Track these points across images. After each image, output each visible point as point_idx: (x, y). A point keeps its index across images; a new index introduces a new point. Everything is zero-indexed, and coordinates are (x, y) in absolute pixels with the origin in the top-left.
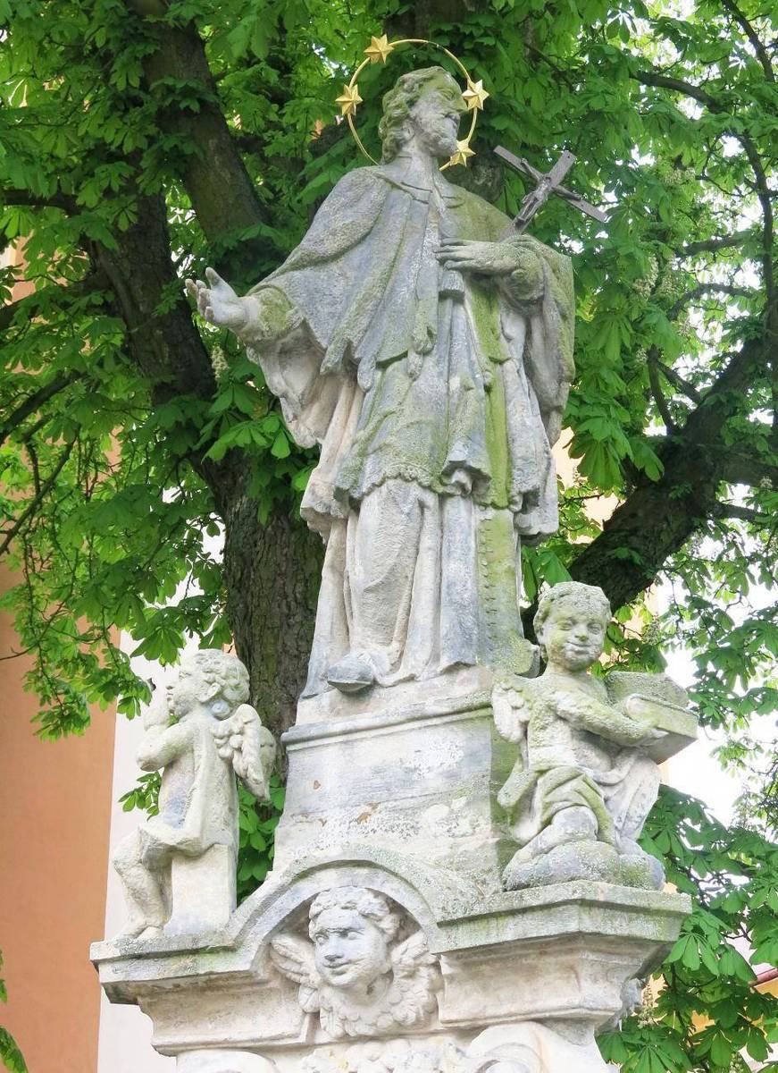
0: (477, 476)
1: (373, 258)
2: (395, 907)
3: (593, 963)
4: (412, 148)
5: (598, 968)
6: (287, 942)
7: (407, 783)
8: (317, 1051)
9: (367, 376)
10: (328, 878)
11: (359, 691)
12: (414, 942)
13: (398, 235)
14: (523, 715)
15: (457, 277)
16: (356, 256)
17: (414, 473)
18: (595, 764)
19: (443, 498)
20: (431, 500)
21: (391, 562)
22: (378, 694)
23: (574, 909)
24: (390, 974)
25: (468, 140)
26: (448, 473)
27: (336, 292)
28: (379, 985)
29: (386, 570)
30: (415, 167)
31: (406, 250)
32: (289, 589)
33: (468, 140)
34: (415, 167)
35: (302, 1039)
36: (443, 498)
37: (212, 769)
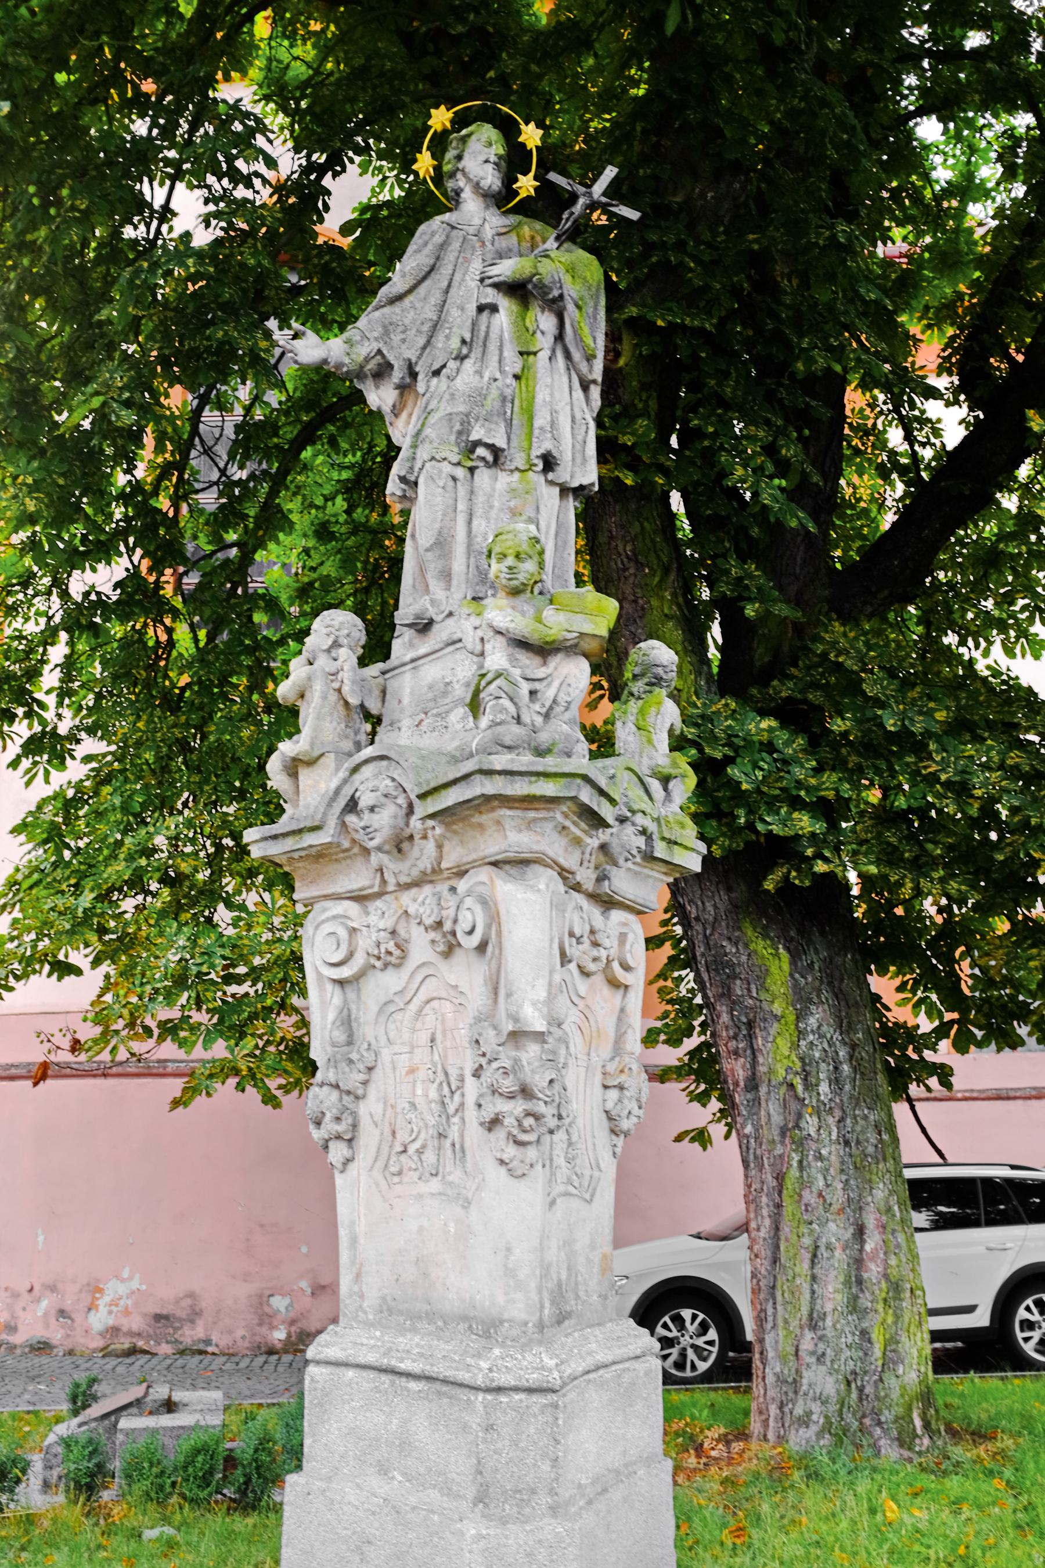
1: (432, 289)
3: (512, 817)
4: (467, 194)
5: (519, 821)
6: (351, 819)
7: (445, 694)
8: (387, 897)
13: (450, 267)
14: (480, 633)
15: (490, 291)
16: (422, 289)
17: (443, 455)
18: (529, 662)
19: (472, 470)
20: (460, 473)
21: (437, 526)
22: (436, 628)
23: (478, 777)
24: (411, 837)
25: (532, 174)
26: (472, 451)
27: (407, 322)
28: (405, 846)
29: (435, 532)
30: (472, 209)
31: (457, 277)
32: (620, 549)
33: (532, 174)
34: (472, 209)
35: (376, 889)
36: (472, 470)
37: (324, 698)
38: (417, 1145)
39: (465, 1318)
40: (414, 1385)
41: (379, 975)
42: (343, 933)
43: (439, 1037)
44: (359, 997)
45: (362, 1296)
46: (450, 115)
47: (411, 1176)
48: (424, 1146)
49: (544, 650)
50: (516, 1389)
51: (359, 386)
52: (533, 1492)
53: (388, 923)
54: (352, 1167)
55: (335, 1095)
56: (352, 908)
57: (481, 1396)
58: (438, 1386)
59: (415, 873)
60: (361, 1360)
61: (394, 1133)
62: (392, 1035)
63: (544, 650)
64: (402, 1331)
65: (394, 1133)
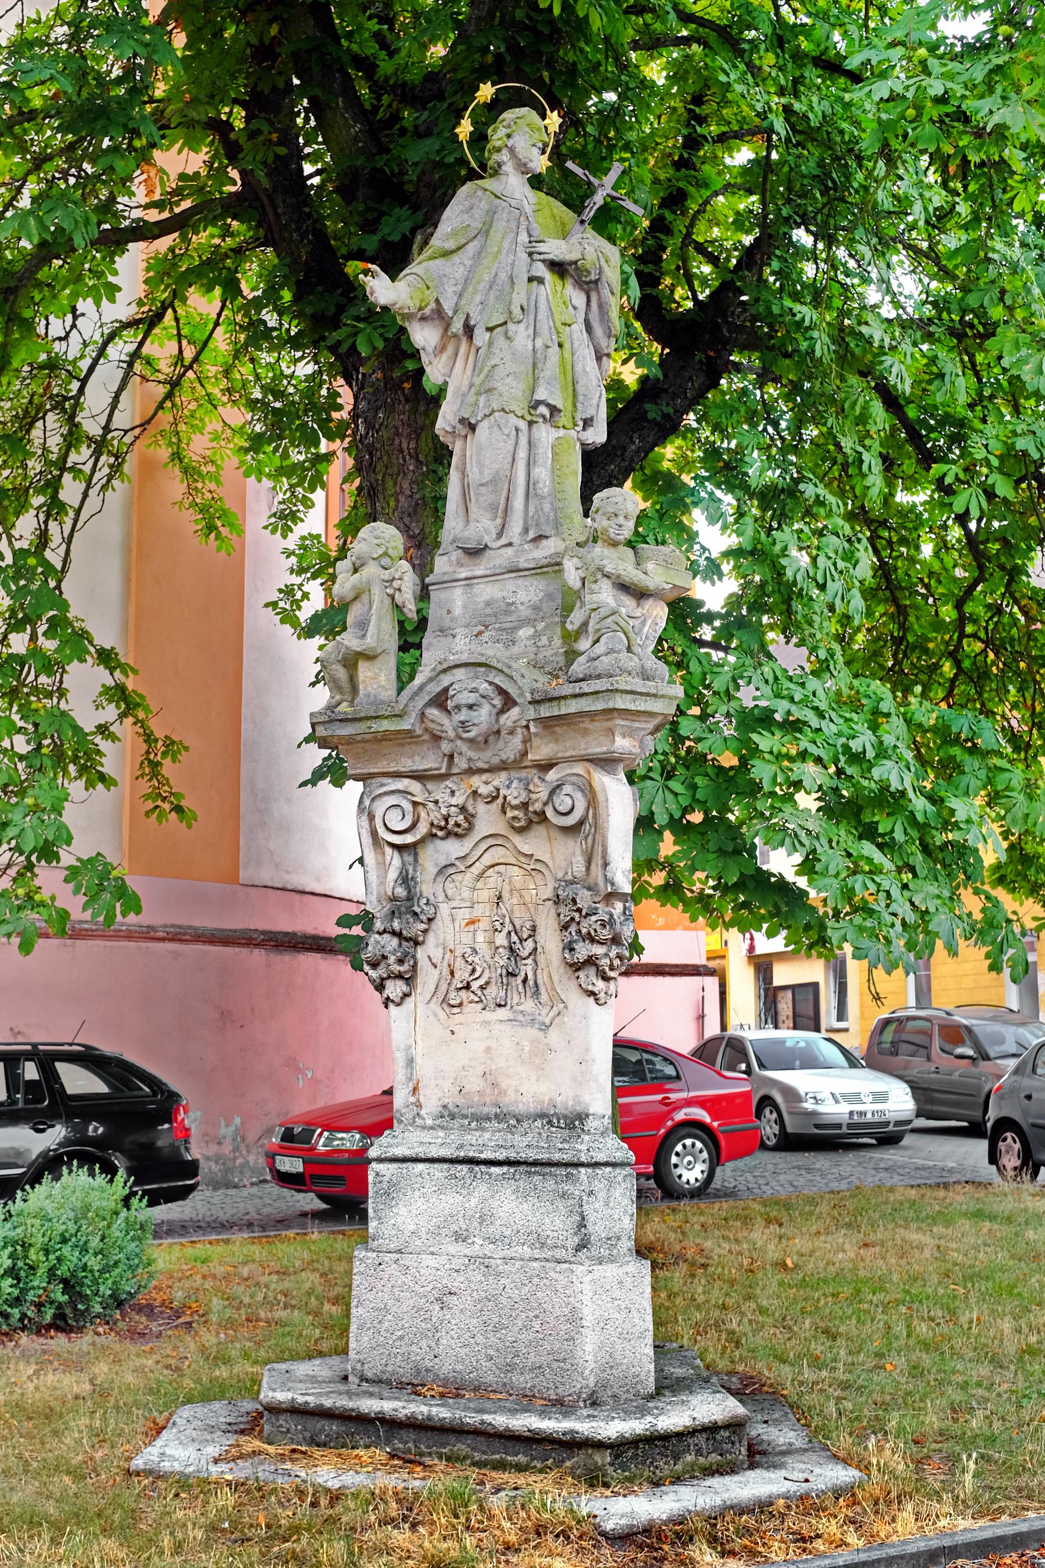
0: (554, 410)
2: (501, 691)
4: (508, 168)
6: (433, 712)
9: (481, 337)
10: (460, 674)
11: (475, 552)
12: (515, 712)
15: (540, 265)
19: (531, 423)
20: (523, 425)
22: (488, 553)
24: (498, 732)
26: (535, 407)
30: (513, 184)
32: (405, 446)
36: (531, 423)
38: (481, 982)
39: (542, 1116)
40: (494, 1170)
41: (439, 842)
42: (408, 806)
43: (506, 895)
44: (416, 860)
45: (420, 1106)
46: (493, 90)
47: (469, 1008)
48: (487, 983)
49: (640, 594)
50: (606, 1164)
51: (407, 325)
52: (619, 1238)
53: (459, 799)
54: (409, 1002)
55: (395, 941)
56: (415, 787)
57: (583, 1170)
58: (522, 1168)
59: (496, 760)
60: (434, 1152)
61: (452, 973)
62: (450, 893)
63: (640, 594)
64: (466, 1129)
65: (452, 973)
